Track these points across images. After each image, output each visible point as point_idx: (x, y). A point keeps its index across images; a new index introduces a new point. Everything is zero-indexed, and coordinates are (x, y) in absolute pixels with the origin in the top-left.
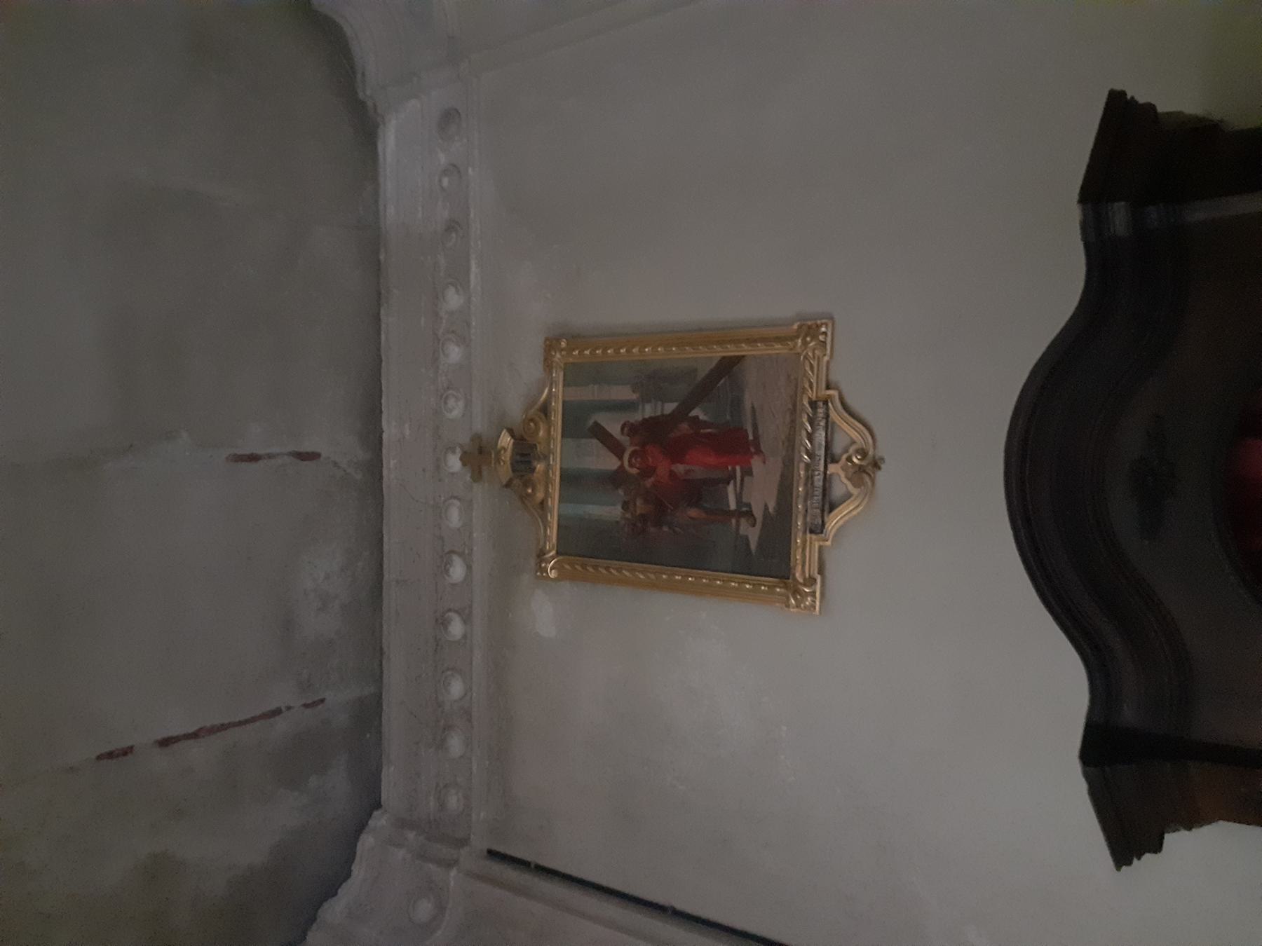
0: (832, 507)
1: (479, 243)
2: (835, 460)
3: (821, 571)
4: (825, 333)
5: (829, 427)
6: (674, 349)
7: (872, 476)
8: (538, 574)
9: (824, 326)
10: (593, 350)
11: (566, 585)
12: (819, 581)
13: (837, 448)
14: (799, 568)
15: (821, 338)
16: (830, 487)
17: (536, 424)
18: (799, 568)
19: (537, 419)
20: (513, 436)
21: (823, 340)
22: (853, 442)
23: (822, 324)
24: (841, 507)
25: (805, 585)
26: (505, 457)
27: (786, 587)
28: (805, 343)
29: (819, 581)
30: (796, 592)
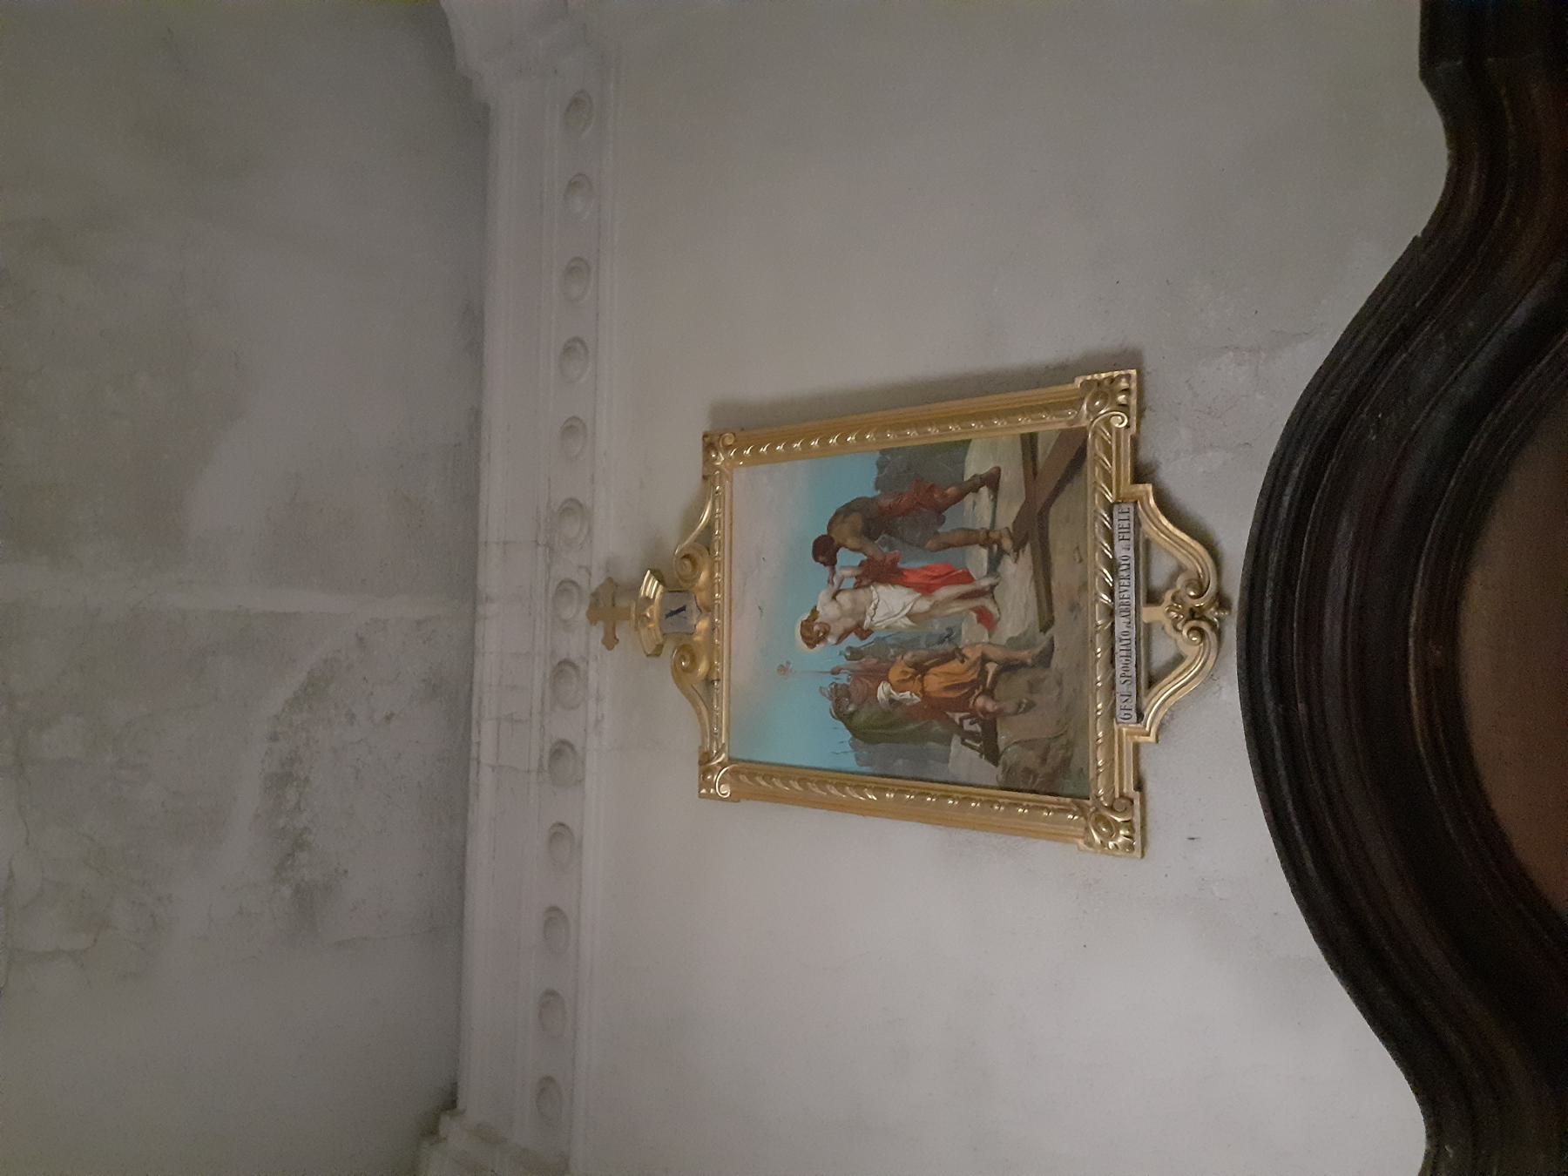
0: (1152, 682)
1: (1467, 268)
2: (1153, 598)
3: (1139, 786)
4: (1127, 391)
5: (1144, 549)
6: (868, 437)
7: (1021, 710)
8: (703, 791)
9: (1124, 380)
10: (859, 434)
11: (746, 806)
12: (1137, 803)
13: (1158, 580)
14: (1101, 781)
15: (1121, 398)
16: (774, 797)
17: (694, 564)
18: (1101, 781)
19: (696, 555)
20: (661, 581)
21: (1125, 402)
22: (1181, 569)
23: (1120, 377)
24: (1165, 681)
25: (1111, 808)
26: (651, 612)
27: (1082, 811)
28: (1093, 412)
29: (1137, 803)
30: (1101, 819)
